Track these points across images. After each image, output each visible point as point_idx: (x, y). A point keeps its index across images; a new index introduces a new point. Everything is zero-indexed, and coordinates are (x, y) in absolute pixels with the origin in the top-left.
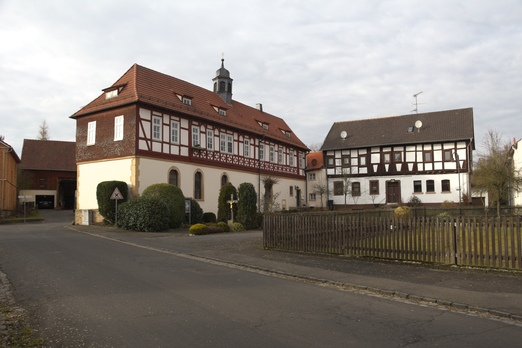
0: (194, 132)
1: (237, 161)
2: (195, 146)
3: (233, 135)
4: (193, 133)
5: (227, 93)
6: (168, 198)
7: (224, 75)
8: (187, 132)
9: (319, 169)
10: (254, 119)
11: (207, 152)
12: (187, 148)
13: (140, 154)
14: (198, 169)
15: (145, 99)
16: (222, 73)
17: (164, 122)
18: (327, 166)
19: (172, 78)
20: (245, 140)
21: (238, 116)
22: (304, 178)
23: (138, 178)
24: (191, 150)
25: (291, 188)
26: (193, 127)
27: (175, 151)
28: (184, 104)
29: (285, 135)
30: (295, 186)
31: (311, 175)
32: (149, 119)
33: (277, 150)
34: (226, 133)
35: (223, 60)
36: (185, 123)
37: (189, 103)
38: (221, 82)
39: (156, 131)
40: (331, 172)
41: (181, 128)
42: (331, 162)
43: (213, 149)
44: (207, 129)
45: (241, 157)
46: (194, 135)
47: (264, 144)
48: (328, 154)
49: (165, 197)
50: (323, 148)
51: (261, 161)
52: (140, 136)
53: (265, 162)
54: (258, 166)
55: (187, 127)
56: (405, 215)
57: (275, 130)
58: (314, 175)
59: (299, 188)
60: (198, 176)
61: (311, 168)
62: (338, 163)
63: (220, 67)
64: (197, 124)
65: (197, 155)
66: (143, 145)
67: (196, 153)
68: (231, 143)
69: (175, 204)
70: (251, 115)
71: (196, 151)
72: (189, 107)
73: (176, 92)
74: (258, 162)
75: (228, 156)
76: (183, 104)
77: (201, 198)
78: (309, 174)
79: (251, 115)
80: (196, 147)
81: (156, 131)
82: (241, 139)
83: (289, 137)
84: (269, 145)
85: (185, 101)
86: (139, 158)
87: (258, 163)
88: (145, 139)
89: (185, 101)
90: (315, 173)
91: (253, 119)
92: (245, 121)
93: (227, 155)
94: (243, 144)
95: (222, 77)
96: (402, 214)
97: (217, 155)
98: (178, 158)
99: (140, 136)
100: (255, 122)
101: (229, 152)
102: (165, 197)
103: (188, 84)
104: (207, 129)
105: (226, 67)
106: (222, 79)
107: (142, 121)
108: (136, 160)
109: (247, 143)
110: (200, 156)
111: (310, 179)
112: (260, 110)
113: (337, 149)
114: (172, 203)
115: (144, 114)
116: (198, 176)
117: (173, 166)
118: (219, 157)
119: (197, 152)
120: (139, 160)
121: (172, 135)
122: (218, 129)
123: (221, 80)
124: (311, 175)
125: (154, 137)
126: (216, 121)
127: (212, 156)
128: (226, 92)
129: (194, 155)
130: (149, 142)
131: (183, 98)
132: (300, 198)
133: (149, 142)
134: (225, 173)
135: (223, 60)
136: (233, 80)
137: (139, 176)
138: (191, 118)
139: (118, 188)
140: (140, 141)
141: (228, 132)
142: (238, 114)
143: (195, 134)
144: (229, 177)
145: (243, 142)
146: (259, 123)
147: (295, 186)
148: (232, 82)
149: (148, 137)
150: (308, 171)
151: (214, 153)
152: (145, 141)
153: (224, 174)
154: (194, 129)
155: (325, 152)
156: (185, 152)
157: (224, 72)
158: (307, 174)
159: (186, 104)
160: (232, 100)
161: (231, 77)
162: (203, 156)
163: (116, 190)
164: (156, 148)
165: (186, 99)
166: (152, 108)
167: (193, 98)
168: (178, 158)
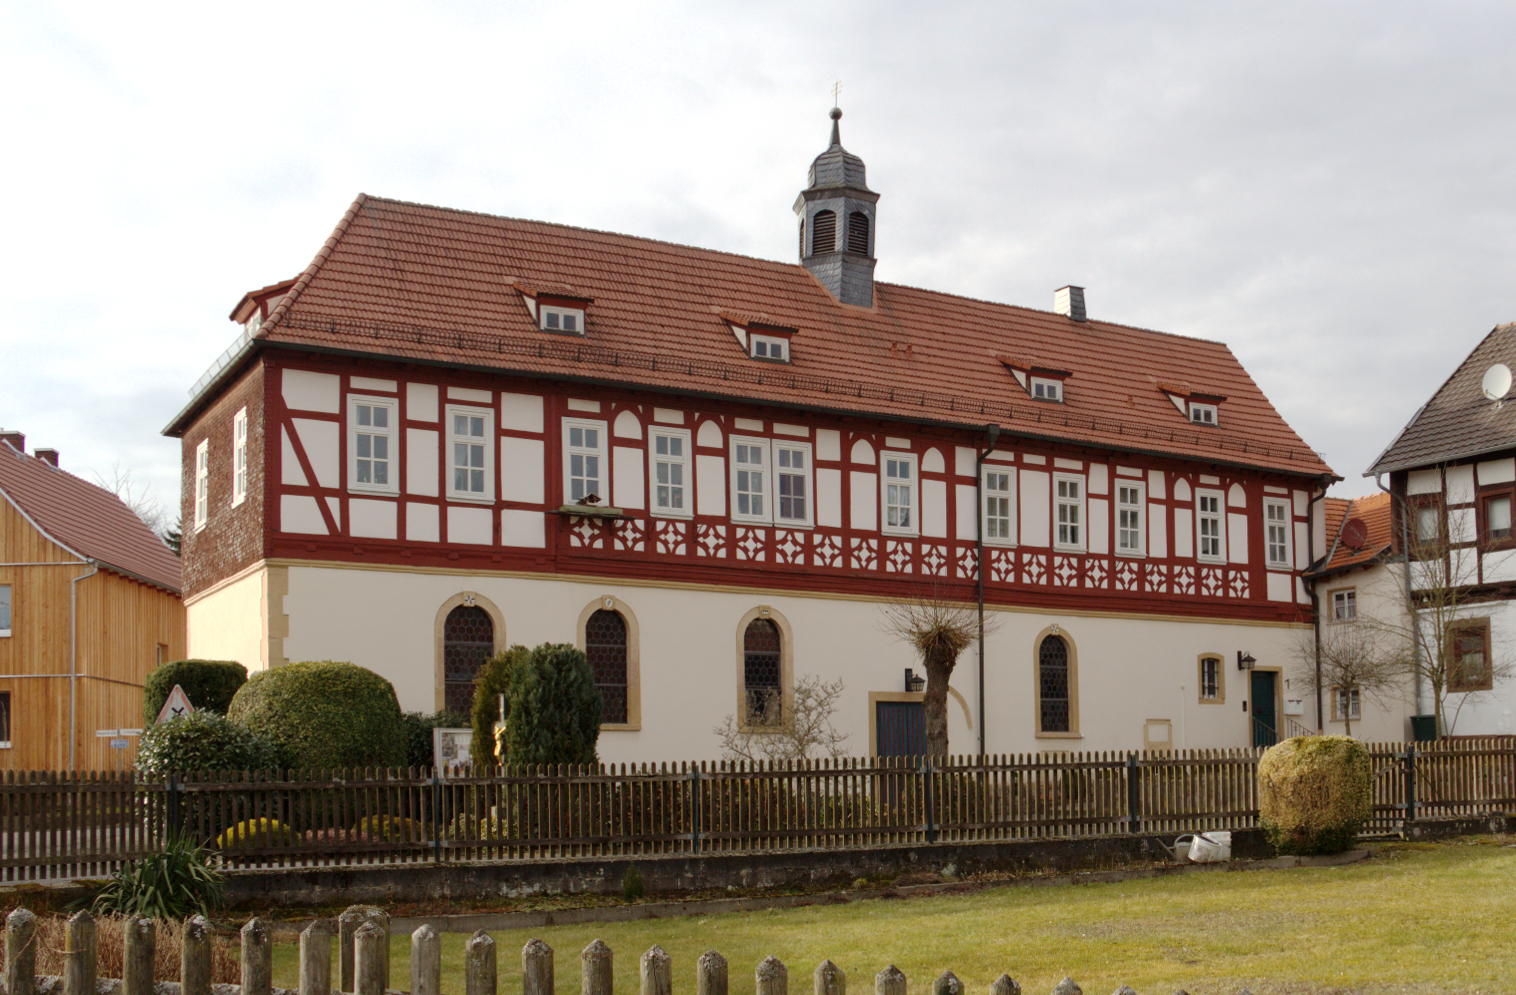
0: (1271, 515)
1: (1104, 574)
2: (582, 502)
3: (1290, 496)
4: (1267, 522)
5: (840, 257)
6: (294, 718)
7: (833, 179)
8: (1105, 503)
9: (1368, 566)
10: (996, 357)
11: (732, 530)
12: (540, 516)
13: (281, 547)
14: (602, 599)
15: (311, 334)
16: (823, 175)
17: (1151, 496)
18: (1405, 547)
19: (930, 296)
20: (1200, 492)
21: (888, 354)
22: (1308, 615)
23: (282, 645)
24: (559, 521)
25: (1210, 666)
26: (567, 424)
27: (470, 528)
28: (1036, 400)
29: (1187, 417)
30: (1239, 653)
31: (1340, 598)
32: (435, 419)
33: (1105, 492)
34: (768, 433)
35: (836, 115)
36: (525, 411)
37: (573, 326)
38: (817, 215)
39: (747, 490)
40: (1422, 574)
41: (1089, 496)
42: (1429, 521)
43: (1221, 558)
44: (651, 428)
45: (1185, 562)
46: (1272, 529)
47: (1014, 469)
48: (1417, 487)
49: (285, 717)
50: (1390, 459)
51: (995, 549)
52: (286, 480)
53: (1020, 550)
54: (974, 569)
55: (538, 427)
56: (1301, 779)
57: (1126, 398)
58: (1352, 596)
59: (1257, 663)
60: (1054, 654)
61: (1341, 562)
62: (1465, 525)
63: (823, 145)
64: (1215, 481)
65: (593, 538)
66: (300, 517)
67: (587, 531)
68: (800, 480)
69: (320, 740)
70: (1142, 370)
71: (586, 522)
72: (580, 341)
73: (730, 318)
74: (976, 551)
75: (780, 535)
76: (542, 332)
77: (628, 718)
78: (1330, 592)
79: (1142, 370)
80: (582, 509)
81: (747, 490)
82: (1182, 490)
83: (1213, 426)
84: (1049, 468)
85: (1040, 388)
86: (286, 567)
87: (974, 557)
88: (314, 490)
89: (1040, 388)
90: (1353, 588)
91: (992, 361)
92: (919, 374)
93: (770, 531)
94: (1190, 512)
95: (822, 191)
96: (1285, 779)
97: (934, 552)
98: (496, 558)
99: (286, 480)
100: (1162, 397)
101: (785, 513)
102: (285, 717)
103: (603, 239)
104: (651, 428)
105: (849, 145)
106: (820, 202)
107: (297, 422)
108: (269, 575)
109: (1209, 504)
110: (609, 545)
111: (1338, 616)
112: (1069, 314)
113: (1484, 450)
114: (306, 738)
115: (303, 389)
116: (1054, 654)
117: (462, 593)
118: (1149, 578)
119: (592, 526)
120: (287, 576)
121: (985, 516)
122: (718, 422)
123: (819, 205)
124: (1340, 598)
125: (1061, 540)
126: (523, 367)
127: (1027, 568)
128: (838, 253)
129: (575, 542)
130: (333, 503)
131: (752, 336)
132: (1276, 708)
133: (333, 503)
134: (766, 609)
135: (836, 115)
136: (878, 196)
137: (287, 636)
138: (556, 391)
139: (183, 687)
140: (287, 501)
141: (778, 428)
142: (890, 345)
143: (1276, 523)
144: (789, 626)
145: (1190, 505)
146: (1016, 373)
147: (1239, 653)
148: (878, 205)
149: (328, 478)
150: (1327, 577)
151: (809, 535)
152: (311, 501)
153: (760, 613)
154: (1271, 508)
155: (1400, 479)
156: (526, 531)
157: (831, 166)
158: (1322, 591)
159: (559, 333)
160: (878, 283)
161: (871, 184)
162: (631, 539)
163: (174, 693)
164: (371, 521)
165: (554, 310)
166: (343, 364)
167: (1070, 374)
168: (496, 558)
